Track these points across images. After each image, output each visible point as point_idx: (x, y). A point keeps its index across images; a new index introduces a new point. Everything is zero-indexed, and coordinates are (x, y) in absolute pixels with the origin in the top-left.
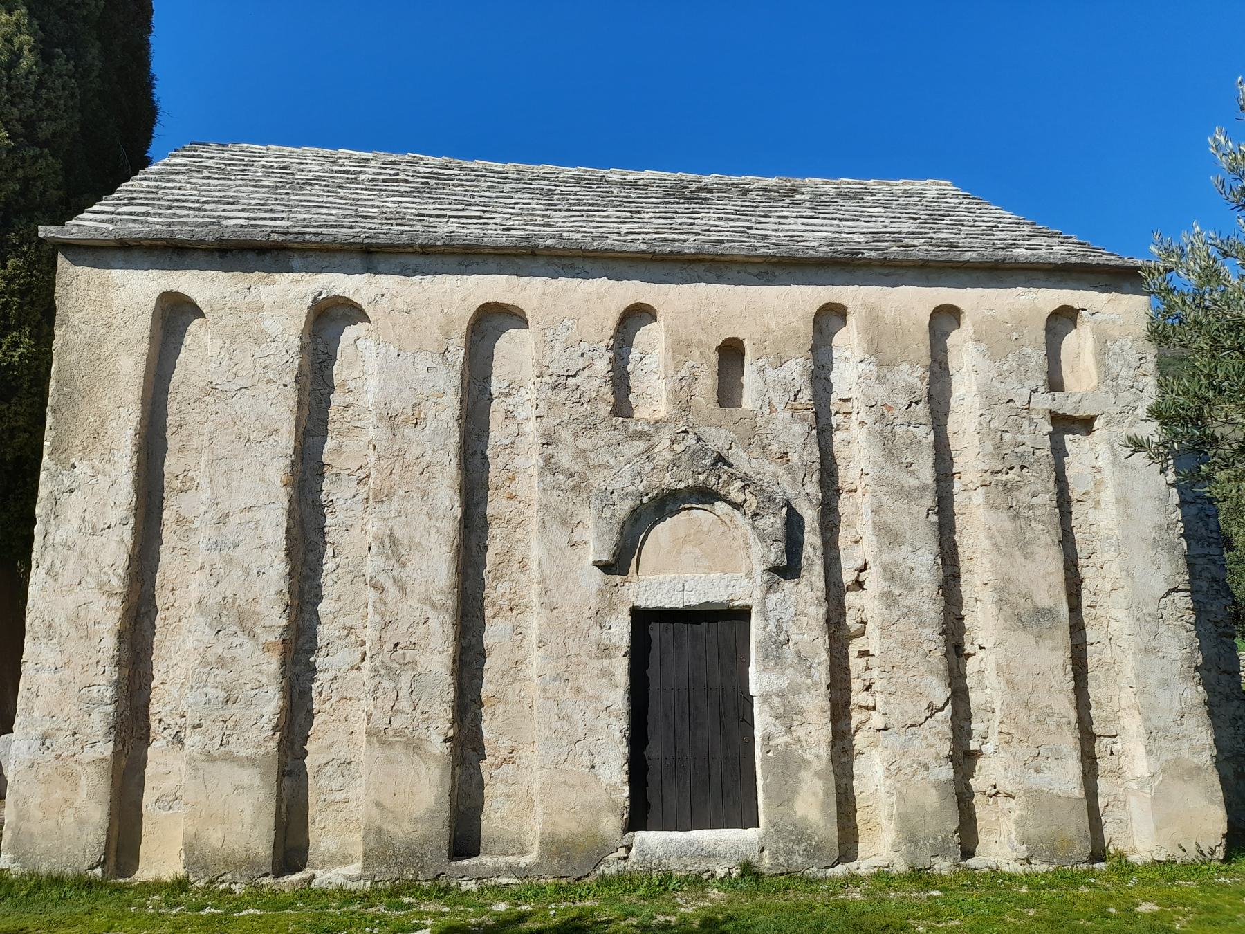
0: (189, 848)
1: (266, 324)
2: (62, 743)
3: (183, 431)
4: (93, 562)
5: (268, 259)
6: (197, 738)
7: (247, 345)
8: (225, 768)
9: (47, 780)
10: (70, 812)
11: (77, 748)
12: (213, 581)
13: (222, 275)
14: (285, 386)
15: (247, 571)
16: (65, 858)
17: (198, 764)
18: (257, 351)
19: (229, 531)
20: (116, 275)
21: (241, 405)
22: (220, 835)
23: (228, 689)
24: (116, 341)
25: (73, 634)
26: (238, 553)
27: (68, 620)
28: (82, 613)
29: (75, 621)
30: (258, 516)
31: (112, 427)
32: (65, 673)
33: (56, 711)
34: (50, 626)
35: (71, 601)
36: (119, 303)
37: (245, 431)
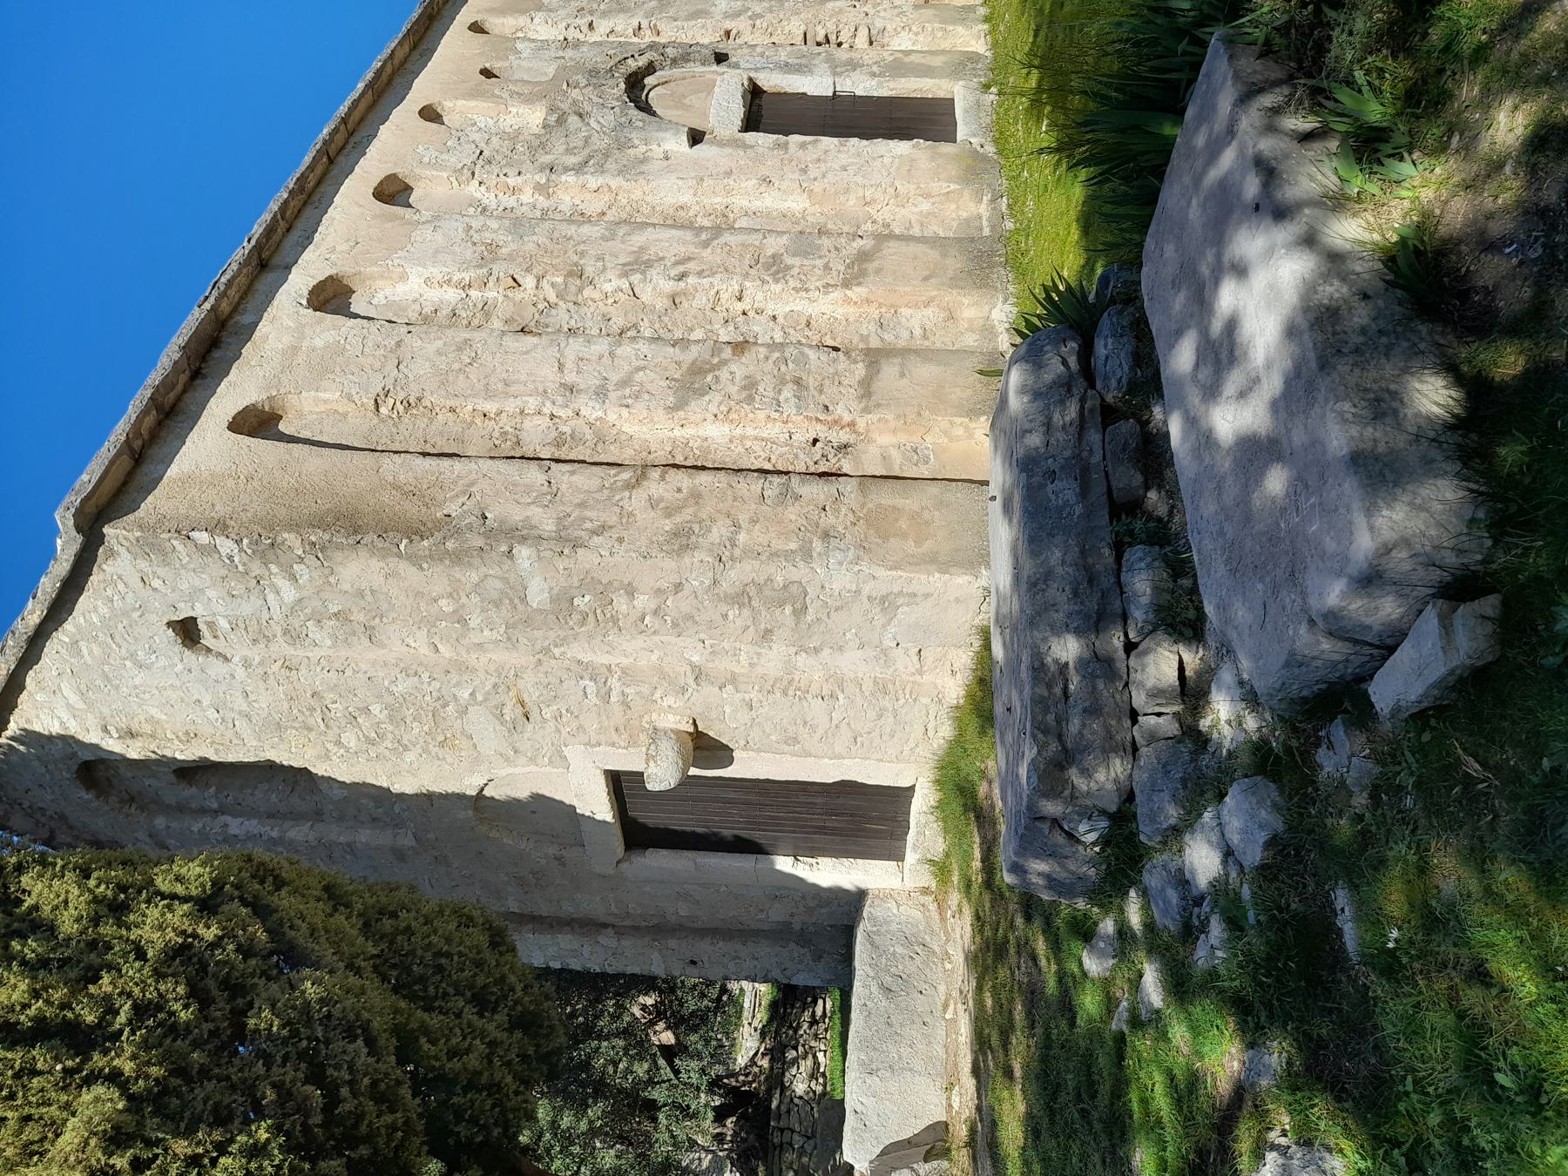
12: (646, 396)
20: (173, 471)
22: (958, 390)
26: (614, 378)
27: (668, 515)
29: (669, 513)
32: (743, 518)
35: (644, 516)
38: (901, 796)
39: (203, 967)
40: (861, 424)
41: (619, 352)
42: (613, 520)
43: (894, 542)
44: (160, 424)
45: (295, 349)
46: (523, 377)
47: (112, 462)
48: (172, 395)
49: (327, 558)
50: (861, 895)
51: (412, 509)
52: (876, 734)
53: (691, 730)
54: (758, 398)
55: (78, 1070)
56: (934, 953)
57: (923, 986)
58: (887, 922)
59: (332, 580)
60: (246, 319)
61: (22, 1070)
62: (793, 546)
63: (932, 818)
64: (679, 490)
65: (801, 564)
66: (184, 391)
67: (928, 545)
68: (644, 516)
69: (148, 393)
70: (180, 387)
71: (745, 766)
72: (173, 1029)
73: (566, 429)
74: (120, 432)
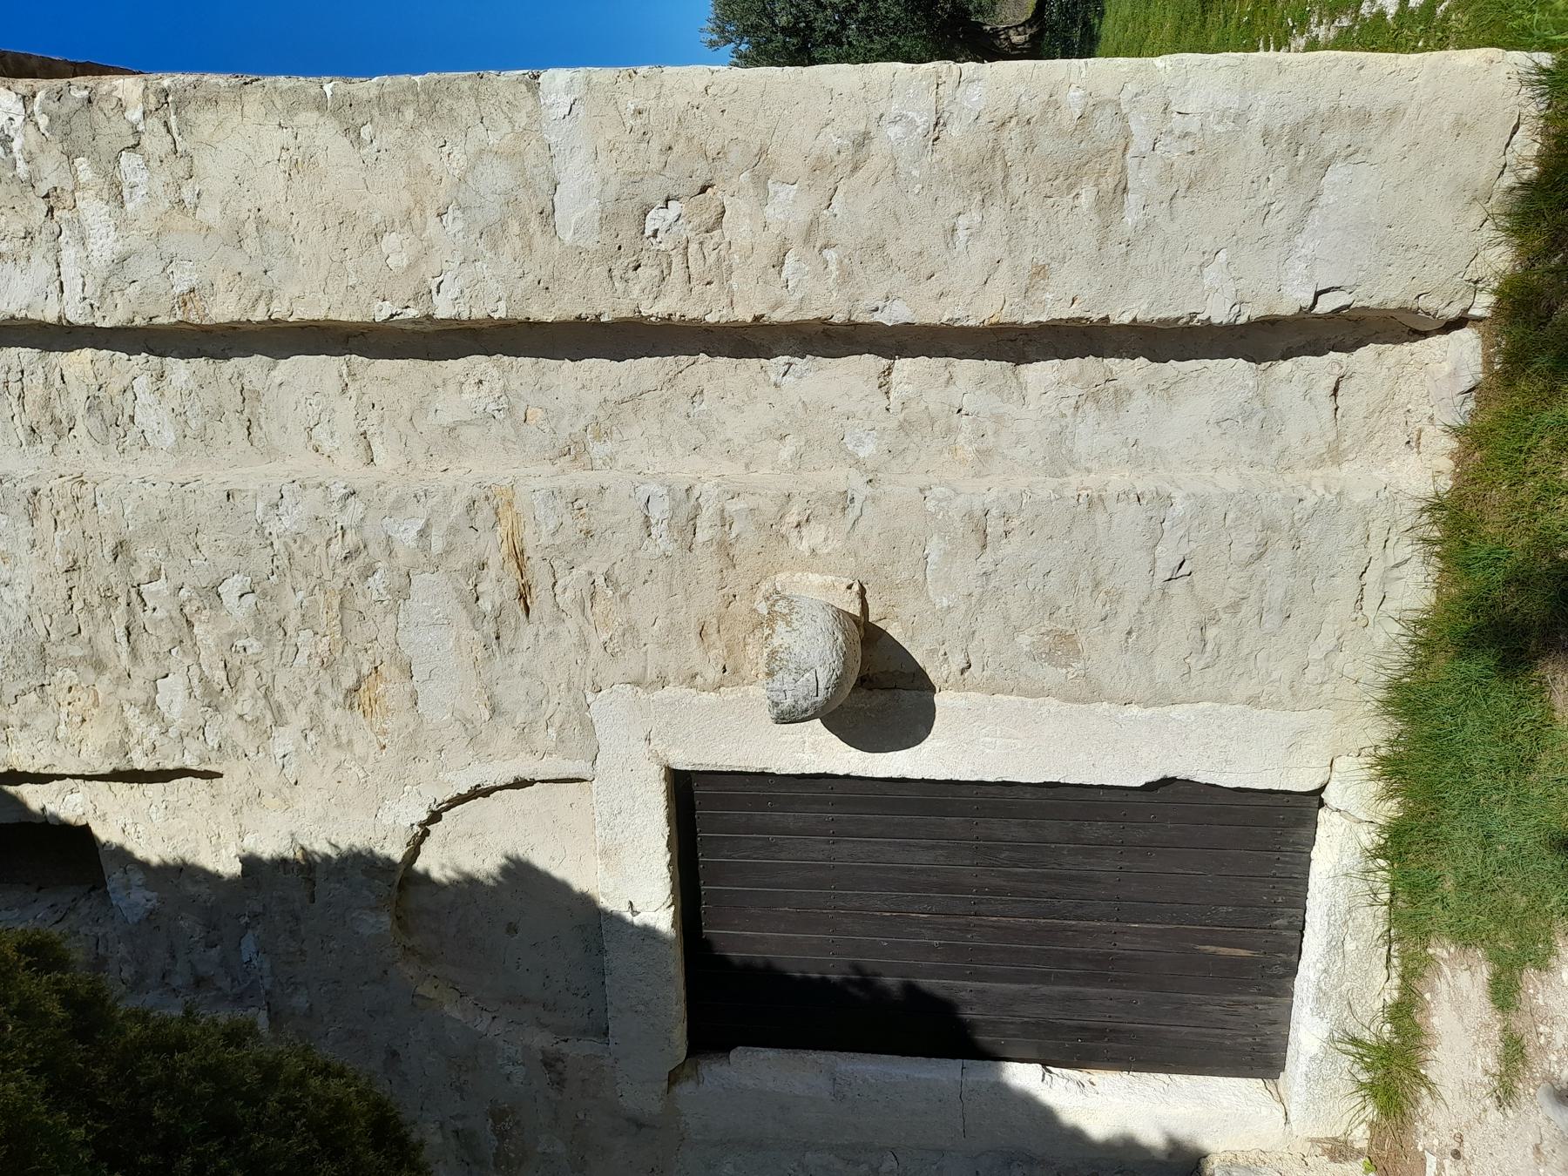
38: (1288, 817)
49: (185, 124)
52: (1246, 610)
53: (855, 609)
59: (187, 194)
63: (1475, 667)
71: (968, 742)
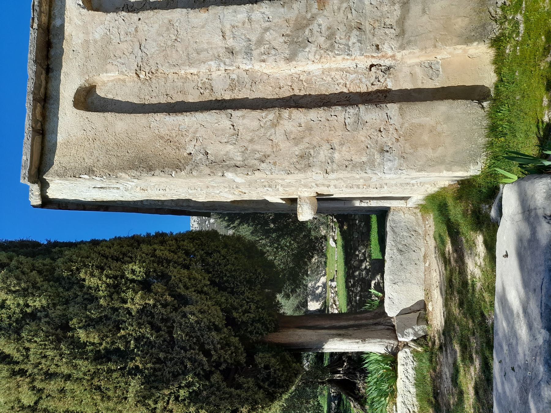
0: (468, 40)
1: (97, 36)
2: (387, 139)
3: (171, 93)
4: (257, 133)
5: (54, 41)
6: (386, 46)
7: (111, 47)
8: (409, 23)
9: (415, 147)
10: (439, 128)
11: (391, 129)
12: (273, 52)
13: (64, 70)
14: (139, 19)
15: (267, 29)
16: (475, 127)
17: (405, 41)
18: (115, 40)
19: (238, 45)
20: (60, 138)
21: (151, 48)
22: (459, 20)
23: (350, 29)
24: (105, 134)
25: (307, 140)
26: (254, 38)
27: (296, 145)
28: (292, 136)
29: (297, 141)
30: (228, 26)
31: (164, 132)
32: (336, 142)
33: (363, 146)
34: (301, 157)
35: (284, 145)
36: (80, 134)
37: (169, 43)
39: (152, 315)
40: (399, 56)
41: (253, 17)
42: (269, 151)
43: (421, 151)
44: (44, 108)
45: (87, 41)
46: (205, 46)
47: (32, 146)
48: (42, 90)
50: (389, 208)
51: (170, 151)
54: (336, 45)
55: (125, 368)
56: (420, 234)
57: (415, 249)
58: (400, 222)
60: (57, 23)
61: (108, 370)
62: (364, 159)
64: (300, 126)
65: (369, 171)
66: (47, 83)
67: (440, 150)
68: (284, 145)
69: (31, 97)
70: (44, 83)
72: (150, 344)
73: (234, 76)
74: (28, 123)
